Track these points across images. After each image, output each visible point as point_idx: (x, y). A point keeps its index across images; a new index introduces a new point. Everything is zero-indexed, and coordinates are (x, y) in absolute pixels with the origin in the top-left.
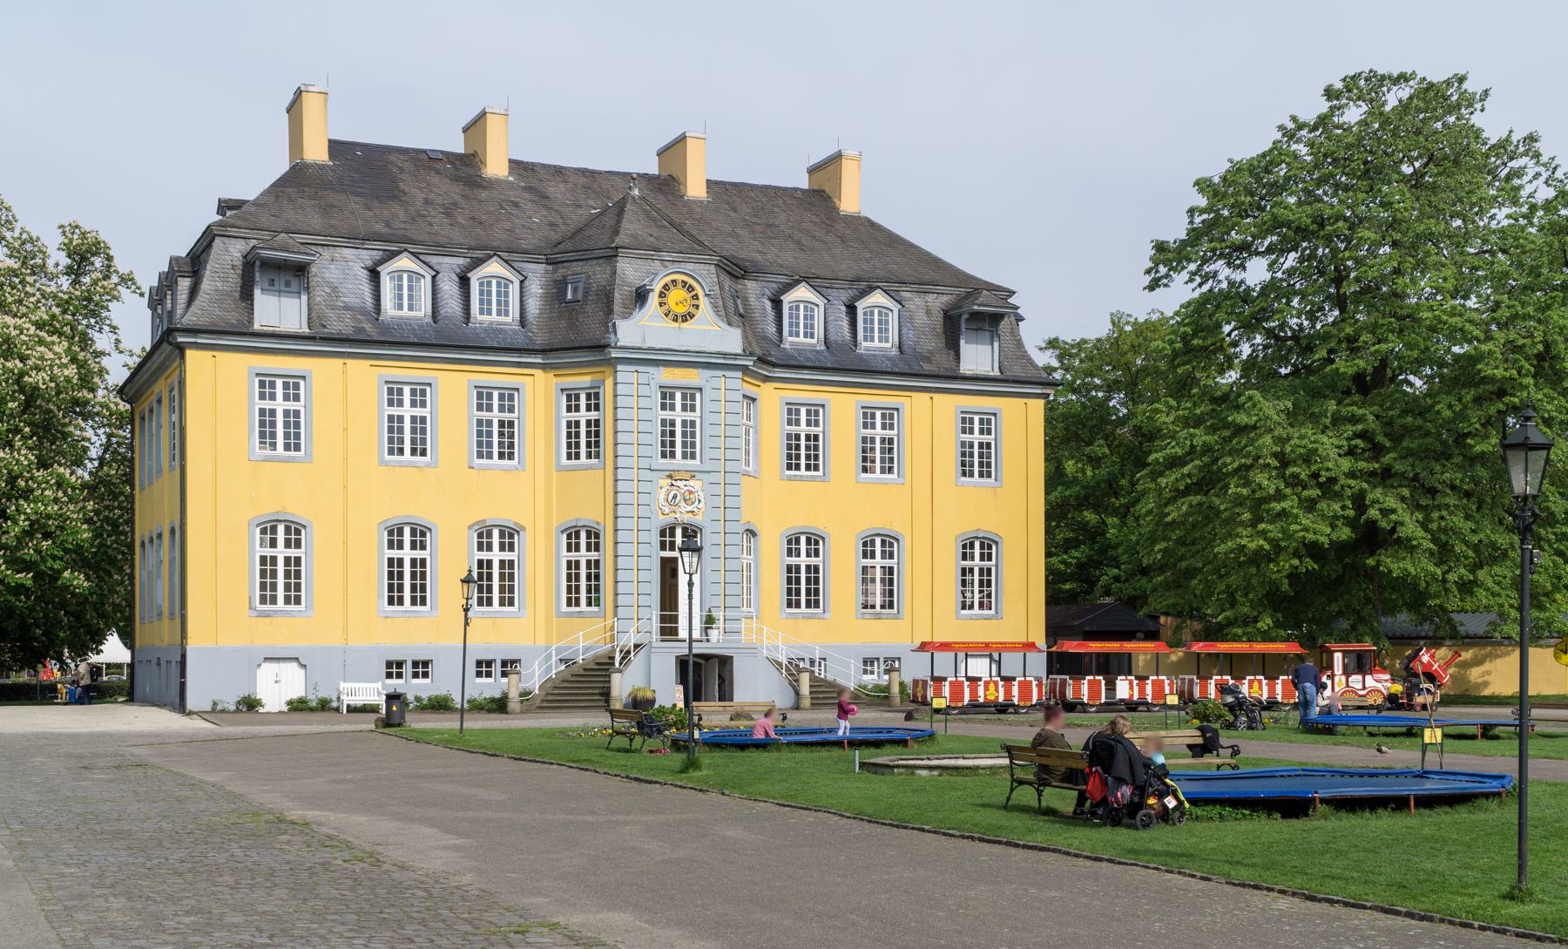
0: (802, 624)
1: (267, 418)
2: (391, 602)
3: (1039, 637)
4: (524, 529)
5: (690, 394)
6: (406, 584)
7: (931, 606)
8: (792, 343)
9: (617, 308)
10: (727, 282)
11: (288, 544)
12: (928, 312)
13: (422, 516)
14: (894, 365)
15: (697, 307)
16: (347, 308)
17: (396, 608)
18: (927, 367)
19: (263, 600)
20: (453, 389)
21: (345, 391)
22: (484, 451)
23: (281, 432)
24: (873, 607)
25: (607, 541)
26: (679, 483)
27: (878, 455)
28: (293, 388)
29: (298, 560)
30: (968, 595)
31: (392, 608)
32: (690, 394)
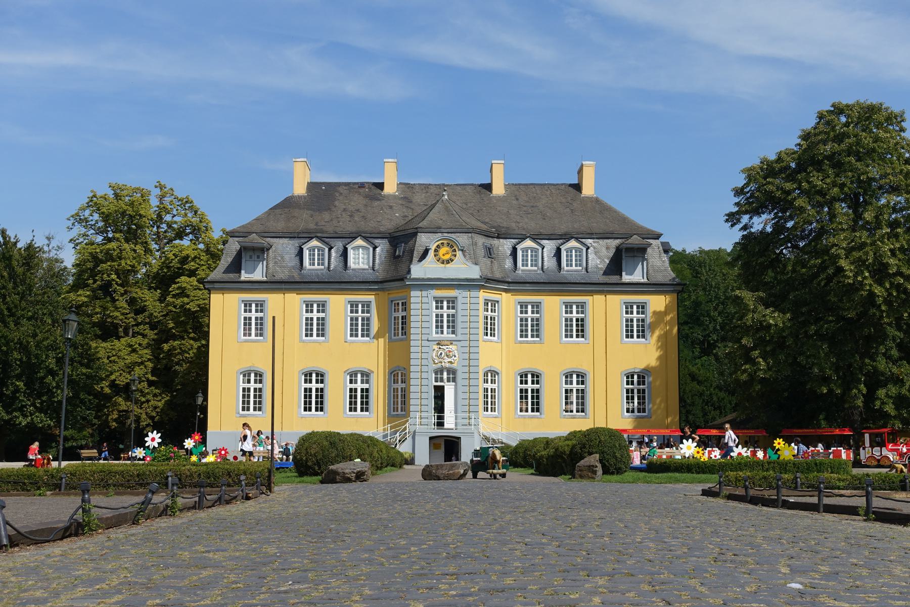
1: (248, 321)
8: (568, 271)
12: (608, 248)
17: (308, 413)
19: (243, 409)
21: (287, 307)
24: (572, 411)
25: (268, 379)
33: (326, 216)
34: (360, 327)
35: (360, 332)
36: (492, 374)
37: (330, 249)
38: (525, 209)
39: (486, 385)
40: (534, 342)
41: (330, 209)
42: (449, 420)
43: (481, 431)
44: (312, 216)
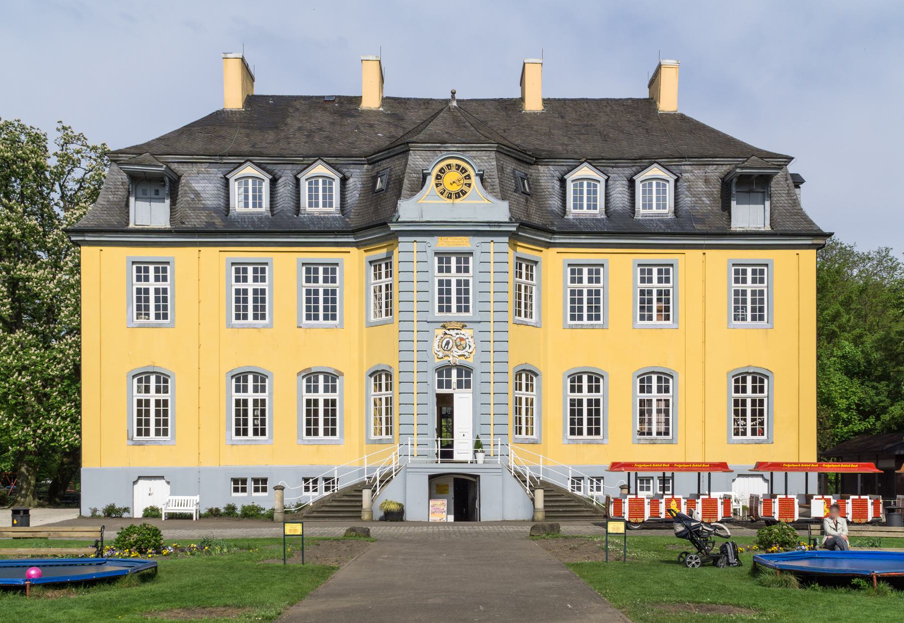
0: (584, 448)
2: (238, 433)
3: (810, 455)
4: (342, 374)
5: (464, 257)
6: (249, 420)
7: (702, 429)
9: (404, 192)
10: (510, 166)
11: (158, 391)
12: (707, 181)
13: (261, 365)
14: (668, 227)
15: (469, 185)
16: (205, 208)
17: (242, 438)
18: (698, 227)
19: (139, 433)
20: (285, 266)
21: (201, 273)
22: (312, 314)
23: (152, 305)
24: (650, 433)
26: (451, 332)
27: (656, 305)
28: (260, 273)
29: (166, 402)
30: (741, 422)
31: (238, 438)
32: (464, 257)
33: (271, 136)
34: (321, 305)
35: (321, 313)
36: (527, 375)
37: (274, 182)
38: (576, 128)
39: (518, 394)
40: (593, 327)
41: (277, 128)
42: (463, 449)
43: (512, 465)
44: (248, 136)
